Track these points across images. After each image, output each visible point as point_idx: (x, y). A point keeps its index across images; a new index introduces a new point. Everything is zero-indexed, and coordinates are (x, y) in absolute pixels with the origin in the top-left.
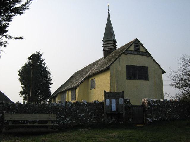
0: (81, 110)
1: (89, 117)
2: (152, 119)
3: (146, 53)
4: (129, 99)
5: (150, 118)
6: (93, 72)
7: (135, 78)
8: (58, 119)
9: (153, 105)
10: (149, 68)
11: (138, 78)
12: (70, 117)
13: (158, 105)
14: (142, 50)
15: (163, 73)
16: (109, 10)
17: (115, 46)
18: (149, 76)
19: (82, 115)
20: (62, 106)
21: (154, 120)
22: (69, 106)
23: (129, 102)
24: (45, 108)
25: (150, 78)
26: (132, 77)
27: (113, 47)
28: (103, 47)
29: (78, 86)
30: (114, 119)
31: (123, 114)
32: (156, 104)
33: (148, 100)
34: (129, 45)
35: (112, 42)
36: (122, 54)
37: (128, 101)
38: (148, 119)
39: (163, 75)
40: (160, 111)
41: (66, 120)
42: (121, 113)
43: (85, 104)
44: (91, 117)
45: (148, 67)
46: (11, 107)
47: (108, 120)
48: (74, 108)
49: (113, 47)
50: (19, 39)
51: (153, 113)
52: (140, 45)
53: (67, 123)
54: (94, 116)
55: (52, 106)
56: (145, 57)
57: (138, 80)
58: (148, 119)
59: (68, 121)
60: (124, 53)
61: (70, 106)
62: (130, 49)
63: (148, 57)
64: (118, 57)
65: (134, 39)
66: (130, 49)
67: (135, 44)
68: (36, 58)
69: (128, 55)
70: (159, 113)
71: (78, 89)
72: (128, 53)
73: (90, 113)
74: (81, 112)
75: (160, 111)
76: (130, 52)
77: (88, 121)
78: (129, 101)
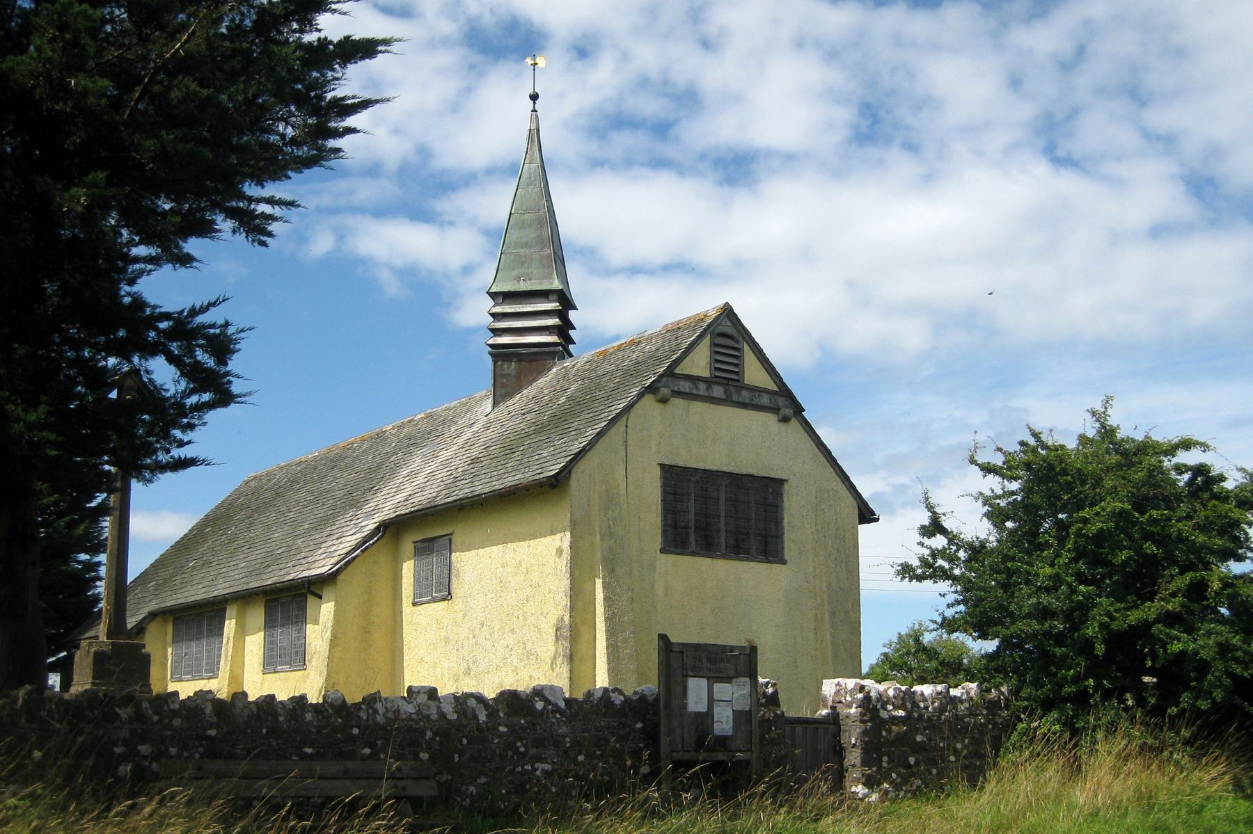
0: (539, 743)
3: (774, 393)
6: (421, 500)
7: (708, 548)
10: (786, 486)
11: (727, 547)
12: (482, 780)
14: (753, 374)
16: (534, 97)
18: (788, 537)
19: (541, 767)
20: (442, 715)
22: (475, 717)
23: (773, 700)
24: (356, 731)
25: (789, 552)
26: (692, 538)
27: (553, 339)
29: (329, 579)
31: (748, 762)
33: (862, 688)
36: (640, 396)
39: (864, 529)
40: (918, 749)
43: (557, 709)
45: (781, 482)
46: (177, 722)
48: (502, 729)
49: (553, 339)
51: (885, 759)
52: (746, 348)
55: (390, 715)
56: (770, 419)
57: (723, 557)
60: (651, 389)
61: (482, 717)
62: (685, 368)
63: (785, 420)
64: (619, 415)
69: (677, 402)
71: (327, 609)
72: (678, 394)
76: (685, 386)
78: (775, 693)
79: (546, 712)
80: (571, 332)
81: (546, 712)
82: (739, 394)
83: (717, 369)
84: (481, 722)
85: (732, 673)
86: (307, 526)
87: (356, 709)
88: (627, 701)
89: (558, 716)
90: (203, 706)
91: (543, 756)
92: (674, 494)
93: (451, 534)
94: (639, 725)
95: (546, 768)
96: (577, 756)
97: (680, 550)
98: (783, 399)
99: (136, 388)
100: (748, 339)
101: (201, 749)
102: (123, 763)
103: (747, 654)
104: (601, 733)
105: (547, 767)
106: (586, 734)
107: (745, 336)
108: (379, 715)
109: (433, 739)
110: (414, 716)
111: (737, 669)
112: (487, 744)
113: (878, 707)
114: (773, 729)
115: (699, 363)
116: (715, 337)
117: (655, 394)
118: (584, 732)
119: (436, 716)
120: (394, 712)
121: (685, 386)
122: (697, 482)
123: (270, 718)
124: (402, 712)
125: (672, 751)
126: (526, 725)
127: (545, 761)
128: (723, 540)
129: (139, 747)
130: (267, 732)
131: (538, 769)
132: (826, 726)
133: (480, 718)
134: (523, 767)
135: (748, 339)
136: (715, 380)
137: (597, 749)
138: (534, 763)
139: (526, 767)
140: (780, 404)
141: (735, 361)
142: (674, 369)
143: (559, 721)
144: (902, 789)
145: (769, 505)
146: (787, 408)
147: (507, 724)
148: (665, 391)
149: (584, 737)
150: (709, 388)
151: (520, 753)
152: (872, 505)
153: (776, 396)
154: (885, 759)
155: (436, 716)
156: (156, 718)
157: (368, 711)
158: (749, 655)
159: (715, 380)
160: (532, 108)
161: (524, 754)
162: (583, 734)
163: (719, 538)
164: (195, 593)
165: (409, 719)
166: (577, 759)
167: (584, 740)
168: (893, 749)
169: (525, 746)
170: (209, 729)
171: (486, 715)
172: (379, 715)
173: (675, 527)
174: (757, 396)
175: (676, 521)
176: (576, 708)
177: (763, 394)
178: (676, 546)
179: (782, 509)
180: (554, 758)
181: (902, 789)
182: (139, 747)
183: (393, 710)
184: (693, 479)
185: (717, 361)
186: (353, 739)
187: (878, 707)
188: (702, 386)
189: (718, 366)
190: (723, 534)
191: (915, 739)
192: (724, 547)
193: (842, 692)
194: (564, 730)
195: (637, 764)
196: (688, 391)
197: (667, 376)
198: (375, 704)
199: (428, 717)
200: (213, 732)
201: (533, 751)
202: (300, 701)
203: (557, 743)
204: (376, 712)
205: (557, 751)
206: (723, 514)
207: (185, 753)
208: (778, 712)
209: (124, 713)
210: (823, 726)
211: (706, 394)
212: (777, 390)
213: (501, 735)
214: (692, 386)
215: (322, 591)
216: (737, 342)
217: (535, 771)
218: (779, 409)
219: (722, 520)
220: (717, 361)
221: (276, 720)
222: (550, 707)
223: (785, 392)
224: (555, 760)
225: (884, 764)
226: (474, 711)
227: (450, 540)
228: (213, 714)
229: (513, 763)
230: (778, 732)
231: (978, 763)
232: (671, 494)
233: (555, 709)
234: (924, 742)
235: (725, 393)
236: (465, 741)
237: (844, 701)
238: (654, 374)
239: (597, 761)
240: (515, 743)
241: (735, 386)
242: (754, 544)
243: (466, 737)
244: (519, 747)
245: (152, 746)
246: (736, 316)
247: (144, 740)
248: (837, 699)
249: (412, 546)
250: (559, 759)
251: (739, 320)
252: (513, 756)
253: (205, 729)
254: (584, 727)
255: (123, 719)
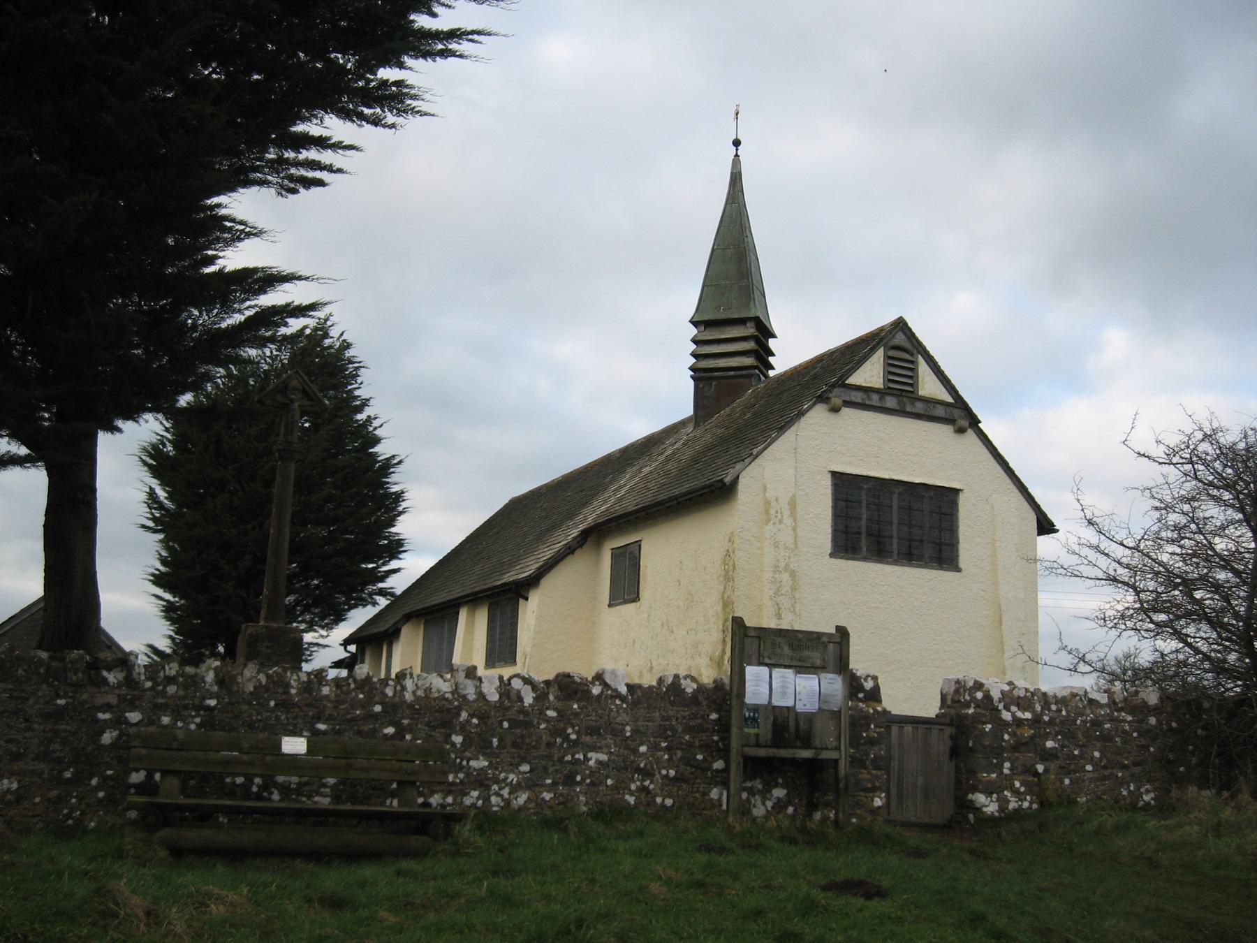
1: (638, 770)
2: (1003, 802)
4: (875, 678)
5: (989, 794)
6: (630, 505)
7: (880, 553)
8: (121, 741)
9: (1007, 716)
10: (961, 494)
11: (899, 553)
12: (525, 768)
13: (1037, 720)
14: (929, 386)
15: (1040, 534)
16: (737, 143)
17: (763, 354)
19: (594, 757)
20: (481, 696)
21: (1013, 805)
22: (520, 699)
23: (874, 695)
26: (864, 542)
27: (748, 361)
28: (694, 355)
30: (779, 793)
31: (836, 761)
32: (1028, 715)
34: (855, 352)
35: (750, 330)
37: (869, 685)
38: (980, 798)
40: (1047, 756)
41: (502, 783)
42: (825, 755)
43: (618, 695)
44: (647, 773)
45: (956, 492)
47: (744, 795)
49: (748, 361)
50: (738, 152)
51: (1007, 765)
52: (921, 359)
53: (508, 803)
54: (667, 768)
55: (420, 693)
56: (945, 431)
58: (980, 798)
59: (515, 789)
61: (529, 698)
63: (961, 431)
65: (885, 318)
66: (857, 379)
67: (892, 353)
68: (776, 337)
69: (846, 411)
70: (1040, 768)
73: (643, 749)
74: (588, 739)
75: (1047, 756)
76: (857, 397)
77: (631, 800)
78: (876, 688)
79: (603, 697)
80: (771, 359)
81: (603, 697)
82: (913, 404)
83: (890, 381)
84: (526, 704)
85: (818, 662)
86: (531, 538)
87: (382, 685)
88: (701, 689)
89: (618, 702)
90: (205, 674)
91: (598, 745)
92: (847, 501)
93: (640, 541)
94: (714, 716)
95: (601, 759)
96: (639, 747)
97: (851, 556)
98: (958, 410)
99: (301, 388)
100: (922, 352)
101: (198, 720)
102: (108, 731)
103: (837, 643)
104: (668, 723)
105: (603, 757)
106: (649, 724)
107: (920, 349)
108: (407, 692)
109: (468, 721)
110: (447, 695)
111: (824, 659)
112: (532, 730)
113: (1000, 708)
114: (872, 726)
115: (871, 374)
116: (888, 350)
117: (827, 403)
118: (648, 721)
119: (474, 696)
120: (425, 690)
121: (857, 397)
122: (869, 489)
123: (280, 690)
124: (434, 690)
125: (743, 746)
126: (578, 711)
127: (600, 751)
128: (895, 546)
129: (127, 714)
130: (276, 705)
131: (591, 759)
132: (940, 727)
133: (525, 700)
134: (573, 756)
135: (922, 352)
136: (888, 391)
137: (662, 740)
138: (587, 752)
139: (577, 756)
140: (956, 416)
141: (909, 373)
142: (846, 380)
143: (619, 708)
144: (1026, 799)
145: (943, 514)
146: (963, 419)
147: (557, 708)
148: (836, 401)
149: (647, 726)
150: (881, 399)
151: (572, 741)
152: (1051, 516)
153: (952, 408)
154: (1007, 765)
155: (474, 696)
156: (149, 684)
157: (395, 688)
158: (840, 643)
159: (888, 391)
160: (735, 153)
161: (576, 743)
162: (647, 723)
163: (892, 545)
164: (441, 597)
165: (442, 698)
166: (638, 750)
167: (648, 729)
168: (1017, 754)
169: (578, 733)
170: (209, 699)
171: (533, 697)
172: (407, 692)
173: (847, 533)
174: (931, 408)
175: (847, 527)
176: (640, 694)
177: (938, 406)
178: (846, 551)
179: (957, 518)
180: (611, 748)
181: (1026, 799)
182: (127, 714)
183: (424, 687)
184: (865, 487)
185: (890, 373)
186: (376, 716)
187: (1000, 708)
188: (875, 397)
189: (891, 377)
190: (895, 541)
191: (1045, 744)
192: (896, 553)
193: (962, 690)
194: (623, 718)
195: (34, 716)
196: (860, 401)
197: (839, 386)
198: (404, 680)
199: (464, 697)
200: (212, 703)
201: (587, 739)
202: (318, 674)
203: (617, 732)
204: (404, 688)
205: (615, 740)
206: (895, 521)
207: (179, 723)
208: (879, 709)
209: (112, 677)
210: (937, 727)
211: (879, 405)
212: (953, 402)
213: (548, 720)
214: (864, 396)
215: (528, 592)
216: (912, 355)
217: (588, 761)
218: (955, 421)
219: (895, 527)
220: (890, 373)
221: (287, 693)
222: (609, 692)
223: (960, 404)
224: (613, 750)
225: (1006, 771)
226: (519, 692)
227: (640, 546)
228: (214, 683)
229: (562, 751)
230: (878, 730)
231: (1120, 775)
232: (843, 500)
233: (614, 694)
234: (1055, 748)
235: (898, 403)
236: (506, 725)
237: (963, 700)
238: (826, 385)
239: (662, 753)
240: (565, 730)
241: (909, 397)
242: (928, 550)
243: (508, 720)
244: (569, 734)
245: (142, 714)
246: (910, 330)
247: (133, 707)
248: (956, 698)
249: (610, 552)
250: (617, 749)
251: (913, 335)
252: (563, 743)
253: (204, 699)
254: (648, 715)
255: (112, 684)
